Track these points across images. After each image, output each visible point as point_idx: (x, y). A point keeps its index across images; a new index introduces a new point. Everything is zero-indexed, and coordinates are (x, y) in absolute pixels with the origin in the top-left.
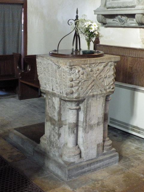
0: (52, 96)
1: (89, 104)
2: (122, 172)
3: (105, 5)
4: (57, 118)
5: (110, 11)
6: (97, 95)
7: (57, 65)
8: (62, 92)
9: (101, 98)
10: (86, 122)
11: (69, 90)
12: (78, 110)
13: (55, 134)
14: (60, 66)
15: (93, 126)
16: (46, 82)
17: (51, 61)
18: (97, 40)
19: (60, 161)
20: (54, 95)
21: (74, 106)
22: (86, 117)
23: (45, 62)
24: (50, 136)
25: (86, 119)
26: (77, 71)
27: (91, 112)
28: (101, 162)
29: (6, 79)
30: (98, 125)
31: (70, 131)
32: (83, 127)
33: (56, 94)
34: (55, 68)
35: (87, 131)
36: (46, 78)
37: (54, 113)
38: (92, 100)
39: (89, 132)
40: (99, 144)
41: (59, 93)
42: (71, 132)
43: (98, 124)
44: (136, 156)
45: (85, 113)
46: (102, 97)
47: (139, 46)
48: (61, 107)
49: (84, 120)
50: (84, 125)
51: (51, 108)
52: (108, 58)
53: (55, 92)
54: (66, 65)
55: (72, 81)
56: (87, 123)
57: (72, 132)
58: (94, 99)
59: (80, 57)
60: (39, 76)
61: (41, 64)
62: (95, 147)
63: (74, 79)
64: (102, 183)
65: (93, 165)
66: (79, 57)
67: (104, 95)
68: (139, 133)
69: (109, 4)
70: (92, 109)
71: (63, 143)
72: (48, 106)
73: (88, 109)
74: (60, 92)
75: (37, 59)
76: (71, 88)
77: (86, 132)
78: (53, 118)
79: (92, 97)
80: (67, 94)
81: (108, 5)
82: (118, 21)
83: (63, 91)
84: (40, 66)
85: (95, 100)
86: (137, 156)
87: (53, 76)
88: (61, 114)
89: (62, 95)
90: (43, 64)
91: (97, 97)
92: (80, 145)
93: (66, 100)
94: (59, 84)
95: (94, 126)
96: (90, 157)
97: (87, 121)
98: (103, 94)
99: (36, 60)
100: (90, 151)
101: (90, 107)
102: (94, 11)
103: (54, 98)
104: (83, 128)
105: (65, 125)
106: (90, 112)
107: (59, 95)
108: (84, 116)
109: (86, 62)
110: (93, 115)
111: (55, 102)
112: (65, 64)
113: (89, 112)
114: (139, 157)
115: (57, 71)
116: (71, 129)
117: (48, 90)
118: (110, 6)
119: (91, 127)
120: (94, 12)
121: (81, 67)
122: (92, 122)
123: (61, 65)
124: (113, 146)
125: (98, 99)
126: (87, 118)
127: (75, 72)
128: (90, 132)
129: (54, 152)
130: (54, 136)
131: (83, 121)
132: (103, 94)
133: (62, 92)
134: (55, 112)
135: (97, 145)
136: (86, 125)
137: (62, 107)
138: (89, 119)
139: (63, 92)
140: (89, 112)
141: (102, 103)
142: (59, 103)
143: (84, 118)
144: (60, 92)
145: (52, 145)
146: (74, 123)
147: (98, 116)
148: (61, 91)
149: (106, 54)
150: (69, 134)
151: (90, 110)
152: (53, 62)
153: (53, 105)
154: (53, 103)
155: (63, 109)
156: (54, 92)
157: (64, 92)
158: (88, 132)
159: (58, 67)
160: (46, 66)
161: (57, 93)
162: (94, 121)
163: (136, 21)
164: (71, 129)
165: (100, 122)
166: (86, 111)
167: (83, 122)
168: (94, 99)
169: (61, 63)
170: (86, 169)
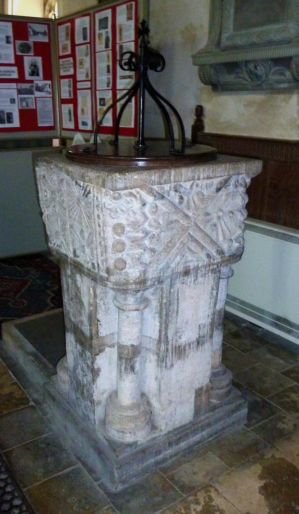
1: (176, 295)
2: (257, 455)
3: (219, 43)
6: (197, 269)
7: (82, 185)
8: (96, 265)
9: (207, 275)
10: (167, 342)
13: (86, 368)
14: (88, 189)
15: (185, 347)
17: (68, 173)
18: (198, 123)
19: (100, 434)
22: (166, 329)
24: (75, 368)
25: (166, 334)
27: (180, 313)
28: (205, 430)
30: (198, 343)
32: (158, 355)
33: (82, 265)
34: (77, 194)
35: (169, 364)
37: (81, 314)
38: (183, 283)
39: (176, 366)
40: (201, 389)
41: (90, 266)
42: (126, 368)
43: (199, 342)
44: (287, 399)
45: (164, 317)
46: (210, 274)
47: (294, 136)
48: (98, 301)
49: (160, 337)
50: (163, 348)
51: (74, 300)
56: (168, 345)
57: (129, 367)
58: (190, 279)
59: (235, 158)
61: (47, 181)
62: (191, 398)
64: (207, 500)
65: (183, 441)
66: (233, 157)
67: (215, 266)
68: (289, 332)
69: (227, 39)
70: (183, 305)
71: (105, 391)
72: (66, 295)
73: (171, 308)
74: (93, 264)
76: (105, 269)
77: (166, 367)
79: (184, 276)
81: (225, 42)
82: (247, 77)
83: (100, 263)
84: (44, 188)
85: (190, 282)
86: (288, 397)
87: (74, 216)
88: (98, 321)
89: (97, 271)
90: (49, 182)
91: (197, 273)
92: (150, 397)
95: (187, 348)
96: (177, 423)
97: (170, 338)
98: (214, 264)
100: (178, 409)
101: (178, 303)
102: (193, 57)
103: (78, 277)
104: (159, 357)
105: (110, 347)
106: (177, 314)
107: (90, 270)
108: (161, 326)
109: (165, 178)
110: (185, 320)
112: (100, 183)
113: (174, 315)
114: (293, 402)
115: (83, 203)
116: (124, 361)
117: (65, 252)
118: (228, 43)
119: (180, 352)
120: (191, 59)
121: (151, 192)
122: (183, 340)
123: (90, 187)
125: (200, 279)
126: (169, 331)
128: (178, 364)
129: (86, 410)
130: (83, 371)
131: (157, 338)
132: (214, 264)
133: (96, 265)
134: (83, 315)
135: (194, 392)
136: (167, 350)
137: (101, 303)
138: (176, 333)
140: (174, 315)
141: (210, 289)
143: (160, 331)
145: (79, 391)
147: (200, 323)
149: (220, 153)
150: (121, 372)
151: (177, 312)
152: (73, 178)
153: (77, 294)
154: (78, 289)
155: (103, 307)
157: (101, 266)
158: (172, 365)
159: (84, 193)
162: (189, 335)
163: (293, 75)
164: (127, 359)
165: (204, 337)
166: (167, 315)
167: (159, 341)
168: (189, 280)
169: (90, 181)
170: (166, 452)
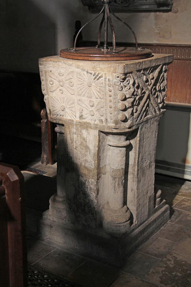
0: (80, 129)
4: (93, 165)
5: (78, 59)
11: (120, 116)
12: (129, 148)
16: (64, 105)
17: (78, 67)
19: (78, 210)
20: (86, 126)
21: (122, 141)
23: (62, 71)
26: (131, 82)
29: (10, 250)
31: (117, 182)
36: (64, 98)
52: (163, 57)
53: (87, 120)
54: (115, 73)
55: (125, 99)
60: (45, 97)
63: (127, 96)
75: (40, 66)
78: (83, 164)
80: (116, 122)
89: (104, 124)
93: (113, 132)
94: (99, 106)
99: (38, 68)
105: (103, 174)
108: (135, 155)
111: (88, 138)
117: (69, 118)
124: (162, 196)
127: (129, 84)
139: (107, 119)
142: (98, 139)
144: (101, 121)
146: (122, 169)
148: (103, 118)
156: (84, 121)
157: (109, 120)
160: (63, 77)
161: (92, 122)
164: (119, 178)
